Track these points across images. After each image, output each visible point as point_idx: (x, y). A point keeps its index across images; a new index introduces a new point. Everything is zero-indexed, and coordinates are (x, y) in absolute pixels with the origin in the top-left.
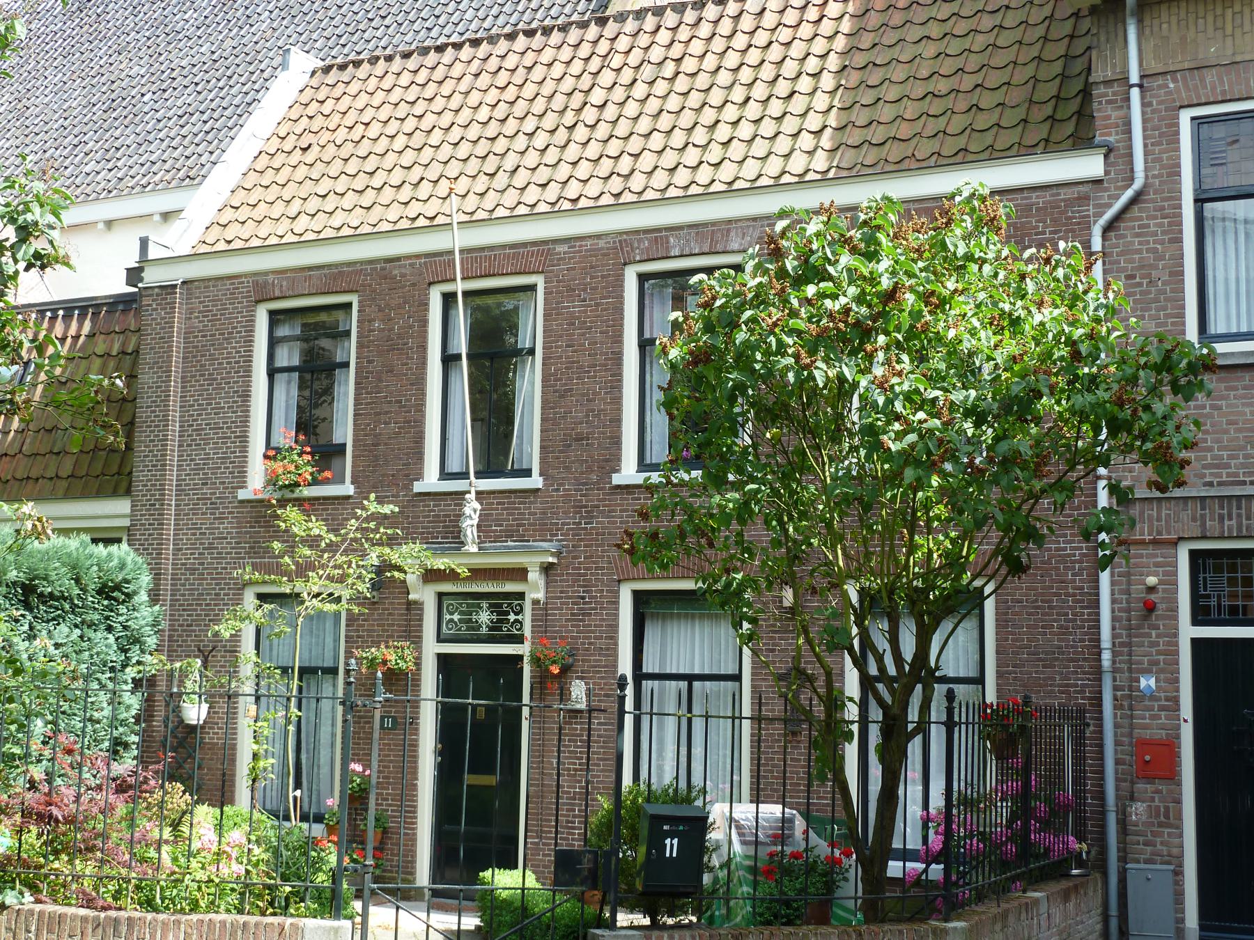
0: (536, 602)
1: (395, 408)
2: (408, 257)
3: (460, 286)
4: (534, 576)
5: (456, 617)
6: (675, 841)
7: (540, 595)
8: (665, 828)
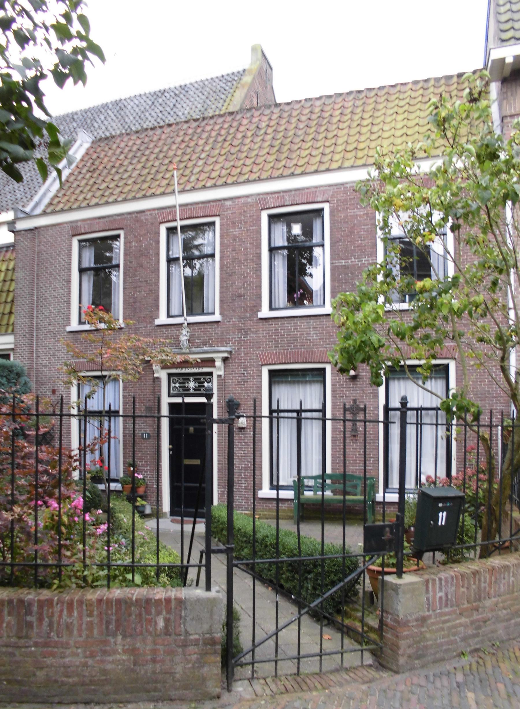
0: (219, 376)
1: (144, 284)
2: (149, 210)
3: (179, 224)
4: (219, 363)
5: (177, 385)
6: (445, 514)
7: (221, 373)
8: (440, 505)
